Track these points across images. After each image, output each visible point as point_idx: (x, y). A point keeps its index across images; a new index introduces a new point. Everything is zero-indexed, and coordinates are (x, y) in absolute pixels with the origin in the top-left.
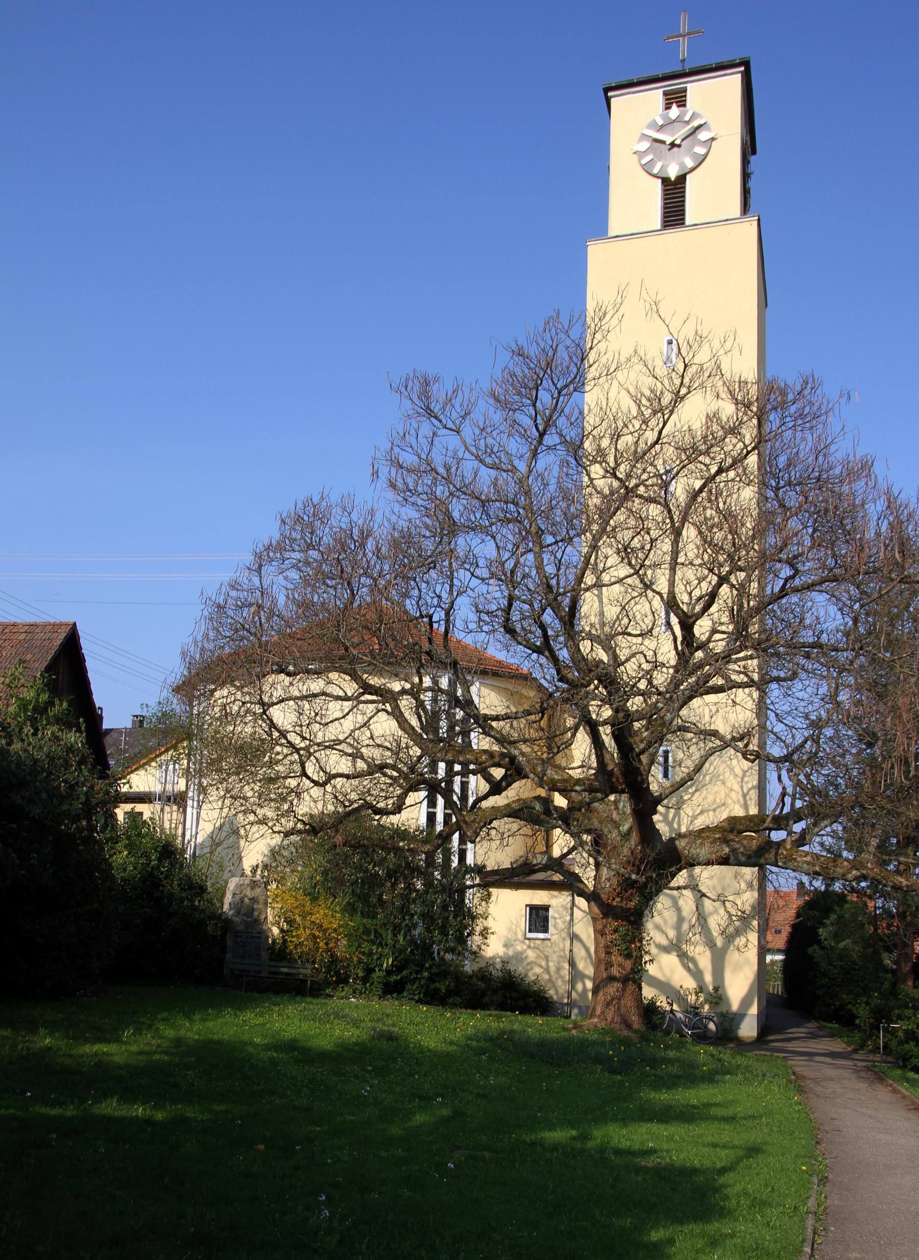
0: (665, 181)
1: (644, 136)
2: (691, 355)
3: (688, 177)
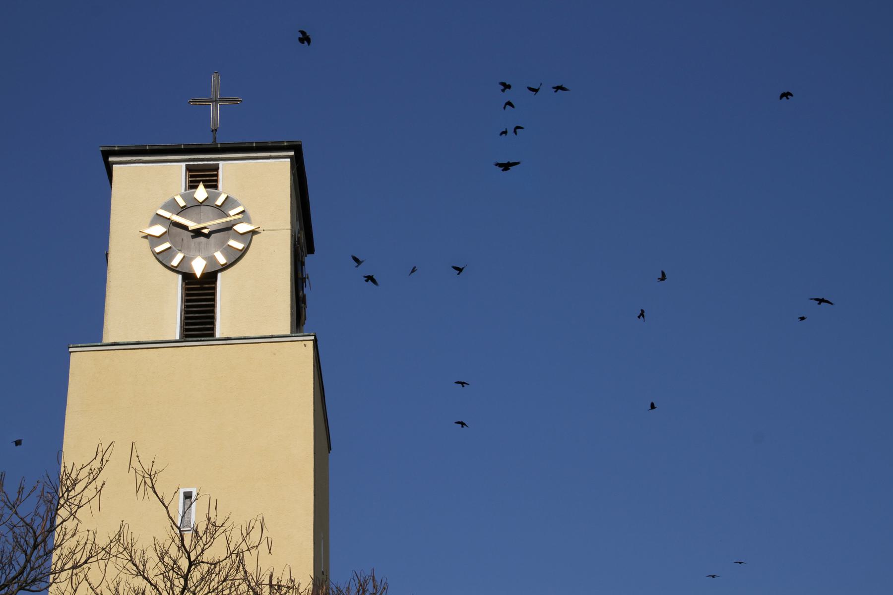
0: (188, 278)
1: (158, 219)
2: (199, 549)
3: (219, 275)
